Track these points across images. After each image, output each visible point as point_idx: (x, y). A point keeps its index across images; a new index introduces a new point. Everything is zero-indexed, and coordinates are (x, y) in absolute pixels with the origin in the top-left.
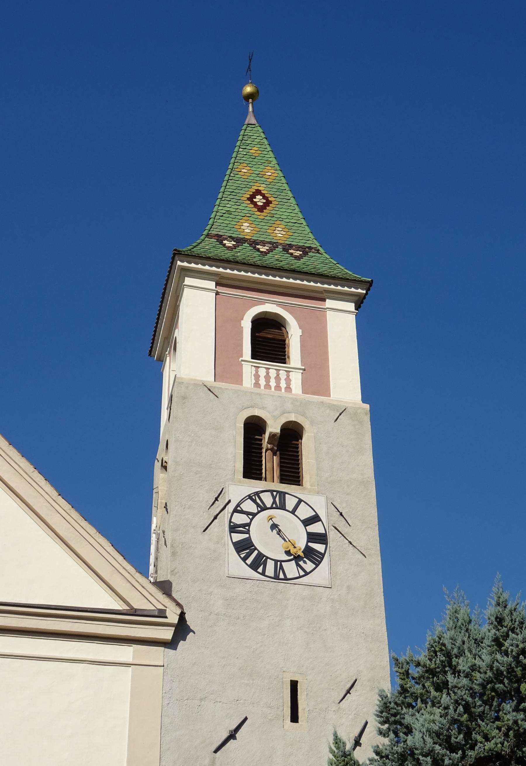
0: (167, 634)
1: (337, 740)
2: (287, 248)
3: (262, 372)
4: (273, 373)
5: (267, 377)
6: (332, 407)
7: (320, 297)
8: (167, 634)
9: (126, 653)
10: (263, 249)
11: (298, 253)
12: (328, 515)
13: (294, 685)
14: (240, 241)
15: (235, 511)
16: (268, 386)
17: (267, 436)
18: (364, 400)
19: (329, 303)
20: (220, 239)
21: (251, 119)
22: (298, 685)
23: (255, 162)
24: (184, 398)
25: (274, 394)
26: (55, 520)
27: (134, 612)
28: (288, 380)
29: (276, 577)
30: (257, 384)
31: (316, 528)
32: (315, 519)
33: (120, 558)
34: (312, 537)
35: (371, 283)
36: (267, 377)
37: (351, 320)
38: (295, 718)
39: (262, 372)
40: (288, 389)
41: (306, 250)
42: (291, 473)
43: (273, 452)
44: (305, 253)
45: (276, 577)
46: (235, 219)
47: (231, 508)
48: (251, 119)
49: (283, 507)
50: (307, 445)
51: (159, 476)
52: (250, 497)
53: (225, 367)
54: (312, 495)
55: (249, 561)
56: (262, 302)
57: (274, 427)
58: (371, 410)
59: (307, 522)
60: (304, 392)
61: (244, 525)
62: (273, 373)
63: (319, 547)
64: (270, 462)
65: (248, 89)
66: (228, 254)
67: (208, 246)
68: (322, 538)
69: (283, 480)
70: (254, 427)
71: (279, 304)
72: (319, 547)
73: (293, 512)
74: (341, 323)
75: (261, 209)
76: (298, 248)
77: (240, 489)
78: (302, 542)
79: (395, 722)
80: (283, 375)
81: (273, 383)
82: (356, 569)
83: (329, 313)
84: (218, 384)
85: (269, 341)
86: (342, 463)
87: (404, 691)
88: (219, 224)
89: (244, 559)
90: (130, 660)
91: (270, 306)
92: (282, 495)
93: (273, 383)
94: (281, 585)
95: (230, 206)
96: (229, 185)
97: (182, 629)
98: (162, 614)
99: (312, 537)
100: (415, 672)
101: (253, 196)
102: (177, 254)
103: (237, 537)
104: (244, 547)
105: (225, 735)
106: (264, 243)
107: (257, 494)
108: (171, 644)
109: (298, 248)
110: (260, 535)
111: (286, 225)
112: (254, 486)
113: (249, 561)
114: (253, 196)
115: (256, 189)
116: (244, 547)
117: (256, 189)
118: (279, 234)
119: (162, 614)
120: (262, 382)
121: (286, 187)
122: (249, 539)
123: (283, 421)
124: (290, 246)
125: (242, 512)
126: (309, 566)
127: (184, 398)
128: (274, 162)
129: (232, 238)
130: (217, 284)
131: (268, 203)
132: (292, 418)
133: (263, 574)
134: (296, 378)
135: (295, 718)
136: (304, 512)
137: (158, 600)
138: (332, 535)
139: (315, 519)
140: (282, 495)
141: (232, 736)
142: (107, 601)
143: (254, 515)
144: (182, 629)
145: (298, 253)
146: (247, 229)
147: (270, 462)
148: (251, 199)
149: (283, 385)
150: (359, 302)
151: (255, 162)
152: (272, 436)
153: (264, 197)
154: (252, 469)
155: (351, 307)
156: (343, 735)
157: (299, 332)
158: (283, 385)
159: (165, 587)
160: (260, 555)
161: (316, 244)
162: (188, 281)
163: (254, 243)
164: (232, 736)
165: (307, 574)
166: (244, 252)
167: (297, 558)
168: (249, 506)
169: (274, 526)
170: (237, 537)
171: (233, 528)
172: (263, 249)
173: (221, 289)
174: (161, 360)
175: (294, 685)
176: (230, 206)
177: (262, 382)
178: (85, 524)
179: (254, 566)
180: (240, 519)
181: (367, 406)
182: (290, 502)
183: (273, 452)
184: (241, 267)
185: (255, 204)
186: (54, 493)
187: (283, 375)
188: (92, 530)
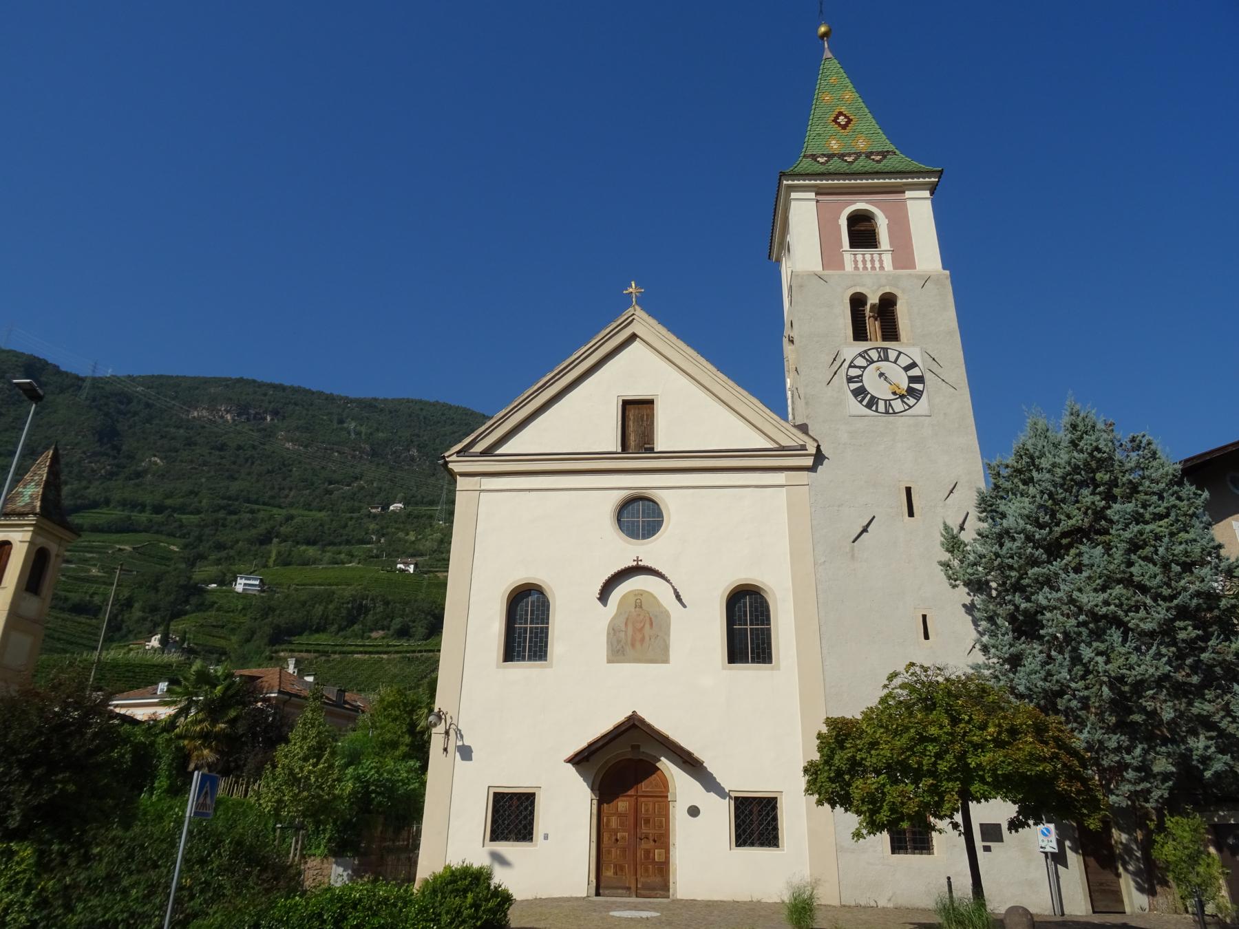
0: (809, 462)
1: (946, 527)
2: (869, 155)
3: (859, 257)
4: (868, 257)
5: (864, 261)
6: (919, 277)
7: (900, 190)
8: (809, 462)
9: (780, 478)
10: (849, 159)
11: (878, 158)
12: (923, 361)
13: (908, 490)
14: (830, 156)
15: (850, 366)
16: (865, 268)
17: (868, 307)
18: (944, 268)
19: (908, 194)
20: (814, 157)
21: (828, 54)
22: (639, 713)
23: (836, 89)
24: (801, 286)
25: (870, 273)
26: (717, 389)
27: (783, 448)
28: (881, 261)
29: (887, 412)
30: (856, 268)
31: (915, 372)
32: (913, 365)
33: (768, 411)
34: (912, 379)
35: (941, 172)
36: (864, 261)
37: (928, 205)
38: (911, 514)
39: (859, 257)
40: (882, 267)
41: (884, 154)
42: (890, 332)
43: (876, 318)
44: (884, 157)
45: (887, 412)
46: (825, 139)
47: (846, 365)
48: (828, 54)
49: (887, 359)
50: (901, 309)
51: (788, 349)
52: (860, 355)
53: (830, 258)
54: (909, 347)
55: (865, 403)
56: (854, 202)
57: (873, 299)
58: (951, 275)
59: (907, 369)
60: (895, 268)
61: (858, 377)
62: (868, 257)
63: (919, 386)
64: (873, 326)
65: (823, 29)
66: (822, 169)
67: (805, 165)
68: (919, 379)
69: (885, 339)
70: (858, 301)
71: (868, 202)
72: (919, 386)
73: (895, 362)
74: (919, 209)
75: (844, 127)
76: (878, 153)
77: (852, 350)
78: (904, 384)
79: (992, 511)
80: (876, 257)
81: (869, 265)
82: (951, 398)
83: (908, 202)
84: (826, 272)
85: (862, 232)
86: (931, 323)
87: (997, 487)
88: (811, 146)
89: (861, 402)
90: (784, 483)
91: (861, 205)
92: (885, 350)
93: (869, 265)
94: (891, 418)
95: (819, 129)
96: (816, 113)
97: (819, 457)
98: (803, 448)
99: (912, 379)
100: (1005, 472)
101: (837, 117)
102: (783, 175)
103: (854, 386)
104: (860, 393)
105: (860, 530)
106: (849, 155)
107: (866, 352)
108: (812, 469)
109: (878, 153)
110: (871, 382)
111: (868, 135)
112: (862, 346)
113: (865, 403)
114: (837, 117)
115: (840, 112)
116: (860, 393)
117: (840, 112)
118: (862, 145)
119: (803, 448)
120: (860, 265)
121: (863, 105)
122: (863, 386)
123: (880, 293)
124: (872, 153)
125: (855, 367)
126: (912, 401)
127: (801, 286)
128: (851, 86)
129: (824, 155)
130: (817, 194)
131: (849, 121)
132: (888, 290)
133: (876, 411)
134: (887, 259)
135: (911, 514)
136: (904, 361)
137: (800, 438)
138: (928, 377)
139: (913, 365)
140: (885, 350)
141: (865, 530)
142: (761, 443)
143: (865, 368)
144: (819, 457)
145: (878, 158)
146: (834, 145)
147: (873, 326)
148: (835, 120)
149: (877, 265)
150: (933, 189)
151: (836, 89)
152: (873, 306)
153: (846, 117)
154: (860, 333)
155: (927, 194)
156: (950, 523)
157: (886, 221)
158: (877, 265)
159: (803, 428)
160: (873, 397)
161: (892, 148)
162: (793, 195)
163: (842, 156)
164: (865, 530)
165: (910, 407)
166: (835, 164)
167: (902, 397)
168: (861, 362)
169: (881, 375)
170: (854, 386)
171: (850, 380)
172: (849, 159)
173: (820, 198)
174: (779, 261)
175: (908, 490)
176: (819, 129)
177: (860, 265)
178: (739, 389)
179: (869, 406)
180: (854, 372)
181: (947, 272)
182: (892, 355)
183: (876, 318)
184: (834, 178)
185: (839, 124)
186: (714, 369)
187: (876, 257)
188: (745, 393)
